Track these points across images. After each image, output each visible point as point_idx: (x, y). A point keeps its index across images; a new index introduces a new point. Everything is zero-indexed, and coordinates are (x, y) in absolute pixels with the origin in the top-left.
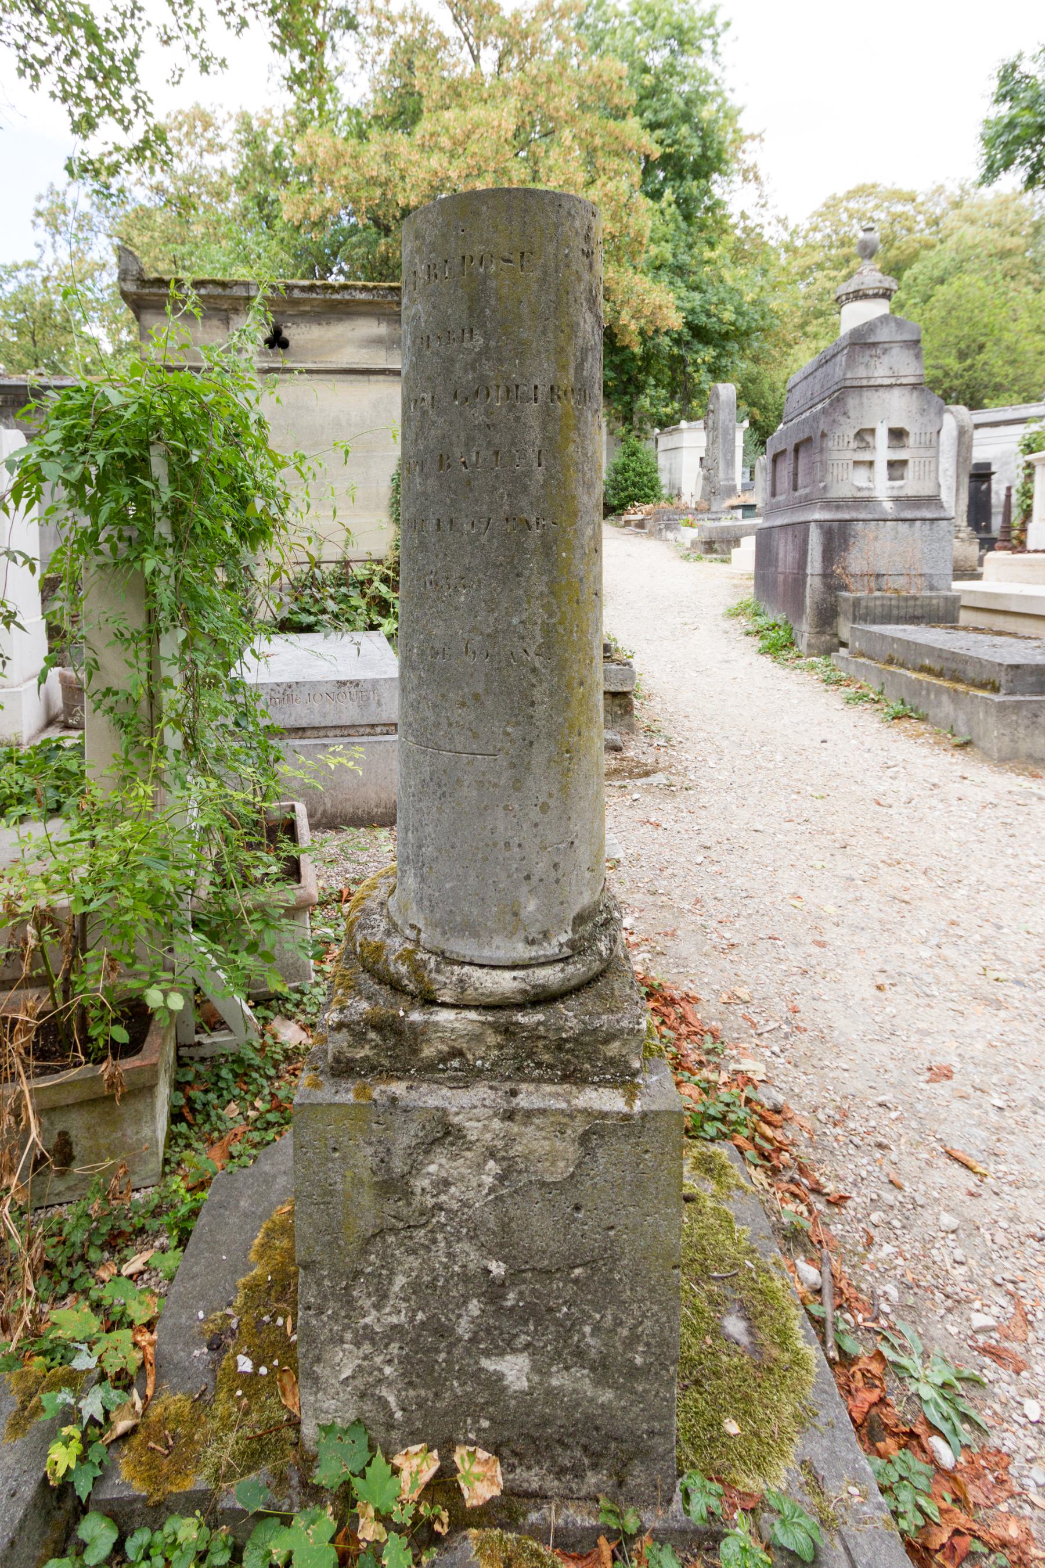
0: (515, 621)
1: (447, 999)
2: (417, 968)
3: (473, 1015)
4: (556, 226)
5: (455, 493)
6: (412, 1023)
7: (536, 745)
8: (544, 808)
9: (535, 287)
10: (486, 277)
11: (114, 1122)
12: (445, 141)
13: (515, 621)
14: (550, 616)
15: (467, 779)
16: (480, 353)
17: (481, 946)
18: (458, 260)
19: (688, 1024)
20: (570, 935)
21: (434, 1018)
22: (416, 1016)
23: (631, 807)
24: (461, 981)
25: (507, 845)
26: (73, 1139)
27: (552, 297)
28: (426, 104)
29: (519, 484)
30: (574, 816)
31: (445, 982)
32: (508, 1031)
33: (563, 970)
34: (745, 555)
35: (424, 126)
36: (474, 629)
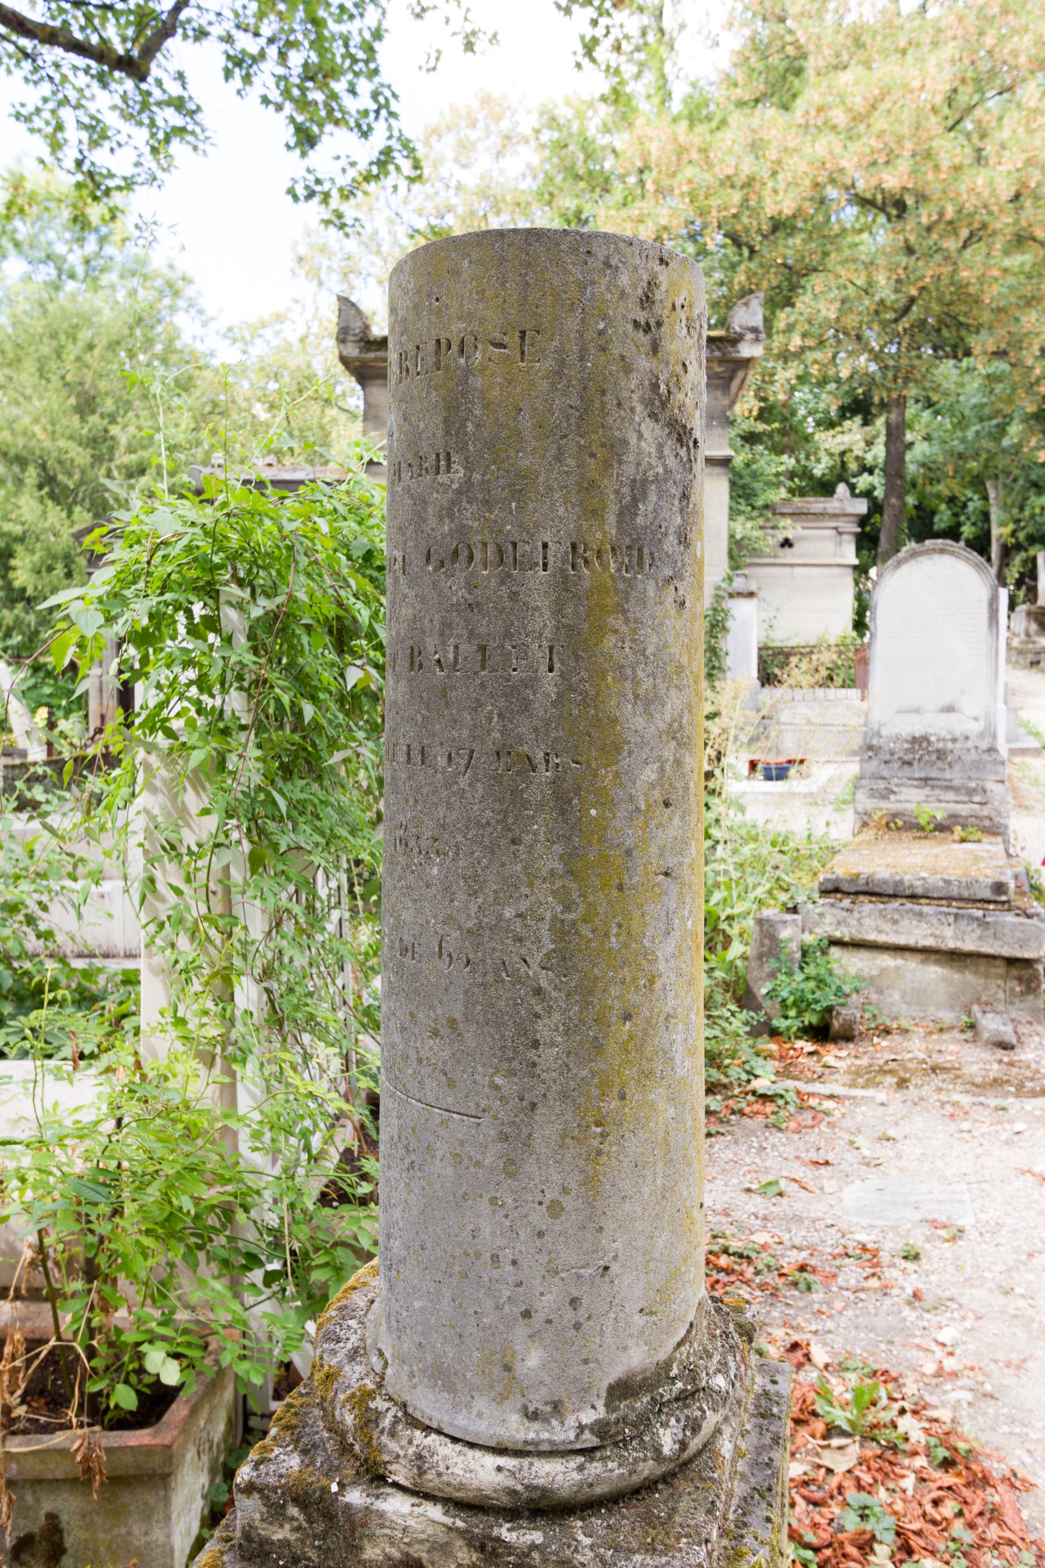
0: (508, 913)
1: (402, 1481)
2: (369, 1420)
3: (435, 1512)
4: (582, 287)
5: (428, 707)
6: (348, 1506)
7: (541, 1110)
8: (555, 1209)
9: (544, 385)
10: (468, 372)
11: (118, 1514)
12: (839, 116)
13: (508, 913)
14: (567, 909)
15: (441, 1148)
16: (459, 492)
17: (456, 1408)
18: (431, 346)
19: (1002, 1524)
20: (601, 1412)
21: (380, 1505)
22: (355, 1497)
23: (1008, 1143)
24: (420, 1457)
25: (495, 1258)
26: (64, 1525)
27: (575, 401)
28: (811, 64)
29: (517, 698)
30: (610, 1226)
31: (398, 1451)
32: (488, 1548)
33: (581, 1468)
35: (811, 94)
36: (449, 919)
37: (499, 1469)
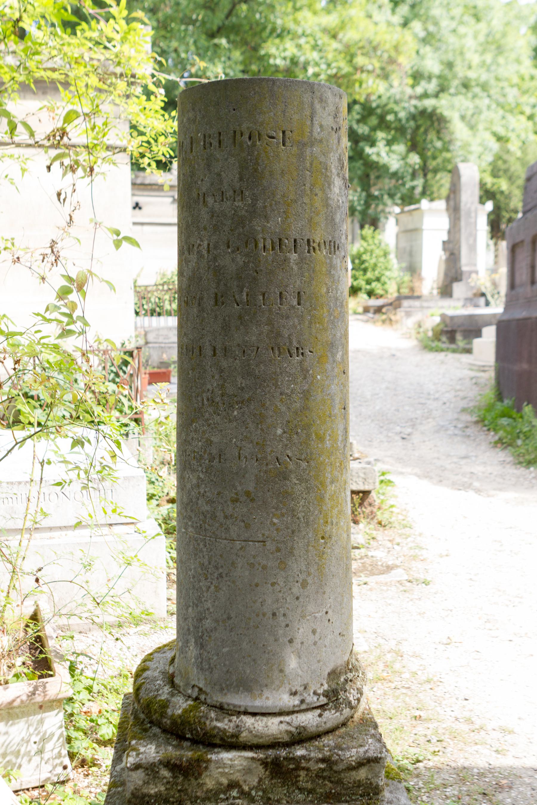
25: (274, 614)
33: (320, 716)
34: (486, 344)
37: (281, 722)
